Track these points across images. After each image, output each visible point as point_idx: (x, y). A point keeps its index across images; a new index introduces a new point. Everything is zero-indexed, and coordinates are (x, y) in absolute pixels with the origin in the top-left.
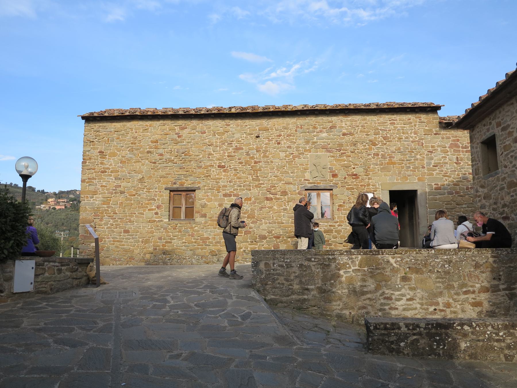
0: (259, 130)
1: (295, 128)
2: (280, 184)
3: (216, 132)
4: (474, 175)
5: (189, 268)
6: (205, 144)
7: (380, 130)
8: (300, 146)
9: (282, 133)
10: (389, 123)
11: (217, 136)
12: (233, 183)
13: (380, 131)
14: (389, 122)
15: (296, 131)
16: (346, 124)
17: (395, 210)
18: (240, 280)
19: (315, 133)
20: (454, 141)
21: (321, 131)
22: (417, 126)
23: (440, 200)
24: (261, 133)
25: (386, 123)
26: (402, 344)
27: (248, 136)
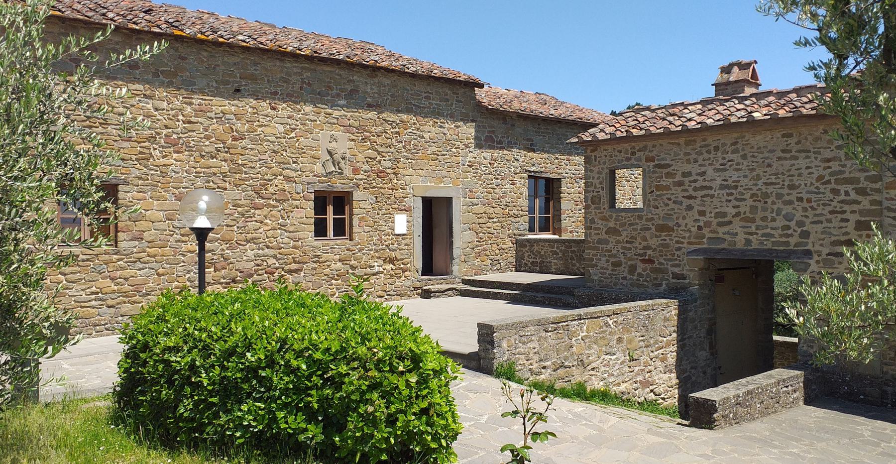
0: (240, 77)
1: (300, 83)
2: (276, 181)
3: (160, 69)
4: (589, 202)
5: (128, 389)
6: (139, 93)
7: (414, 105)
8: (307, 117)
9: (279, 89)
10: (423, 96)
11: (161, 77)
12: (194, 174)
13: (414, 108)
14: (424, 95)
15: (301, 88)
16: (371, 89)
17: (637, 289)
18: (88, 340)
19: (329, 98)
20: (489, 132)
21: (338, 95)
22: (454, 106)
23: (473, 212)
24: (243, 83)
25: (420, 95)
26: (254, 382)
27: (221, 87)
